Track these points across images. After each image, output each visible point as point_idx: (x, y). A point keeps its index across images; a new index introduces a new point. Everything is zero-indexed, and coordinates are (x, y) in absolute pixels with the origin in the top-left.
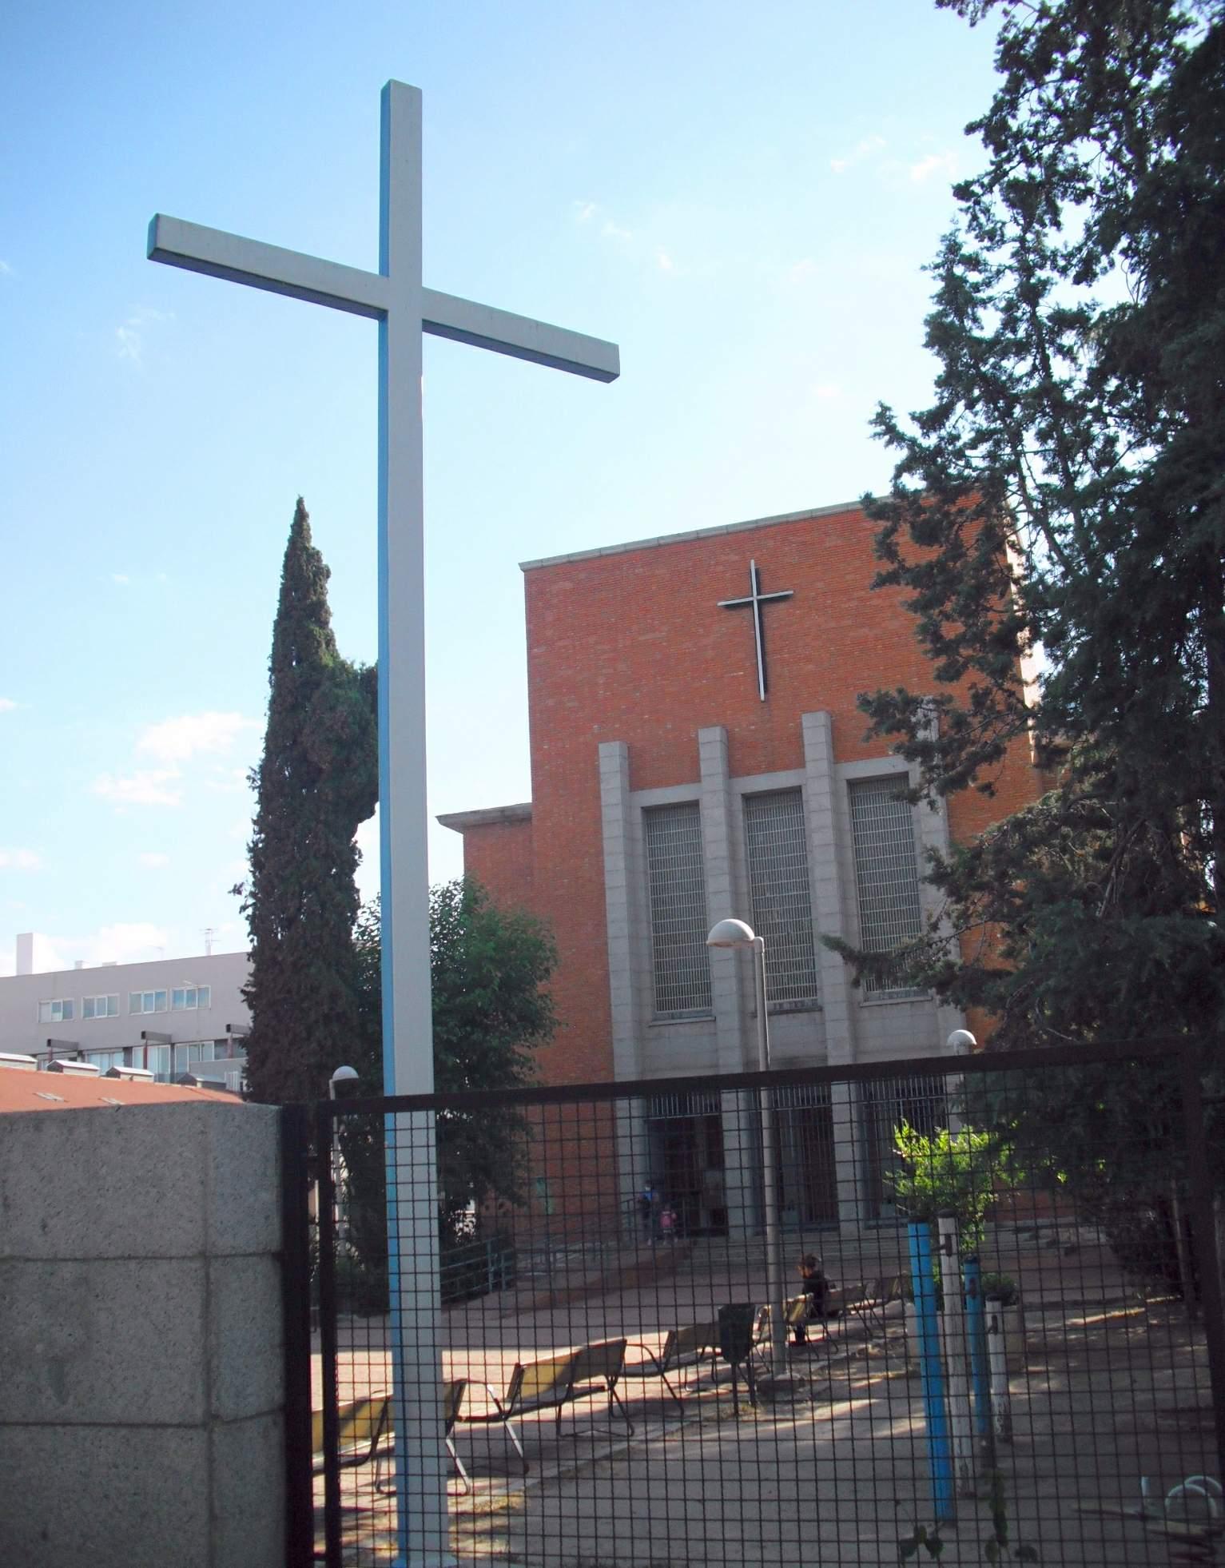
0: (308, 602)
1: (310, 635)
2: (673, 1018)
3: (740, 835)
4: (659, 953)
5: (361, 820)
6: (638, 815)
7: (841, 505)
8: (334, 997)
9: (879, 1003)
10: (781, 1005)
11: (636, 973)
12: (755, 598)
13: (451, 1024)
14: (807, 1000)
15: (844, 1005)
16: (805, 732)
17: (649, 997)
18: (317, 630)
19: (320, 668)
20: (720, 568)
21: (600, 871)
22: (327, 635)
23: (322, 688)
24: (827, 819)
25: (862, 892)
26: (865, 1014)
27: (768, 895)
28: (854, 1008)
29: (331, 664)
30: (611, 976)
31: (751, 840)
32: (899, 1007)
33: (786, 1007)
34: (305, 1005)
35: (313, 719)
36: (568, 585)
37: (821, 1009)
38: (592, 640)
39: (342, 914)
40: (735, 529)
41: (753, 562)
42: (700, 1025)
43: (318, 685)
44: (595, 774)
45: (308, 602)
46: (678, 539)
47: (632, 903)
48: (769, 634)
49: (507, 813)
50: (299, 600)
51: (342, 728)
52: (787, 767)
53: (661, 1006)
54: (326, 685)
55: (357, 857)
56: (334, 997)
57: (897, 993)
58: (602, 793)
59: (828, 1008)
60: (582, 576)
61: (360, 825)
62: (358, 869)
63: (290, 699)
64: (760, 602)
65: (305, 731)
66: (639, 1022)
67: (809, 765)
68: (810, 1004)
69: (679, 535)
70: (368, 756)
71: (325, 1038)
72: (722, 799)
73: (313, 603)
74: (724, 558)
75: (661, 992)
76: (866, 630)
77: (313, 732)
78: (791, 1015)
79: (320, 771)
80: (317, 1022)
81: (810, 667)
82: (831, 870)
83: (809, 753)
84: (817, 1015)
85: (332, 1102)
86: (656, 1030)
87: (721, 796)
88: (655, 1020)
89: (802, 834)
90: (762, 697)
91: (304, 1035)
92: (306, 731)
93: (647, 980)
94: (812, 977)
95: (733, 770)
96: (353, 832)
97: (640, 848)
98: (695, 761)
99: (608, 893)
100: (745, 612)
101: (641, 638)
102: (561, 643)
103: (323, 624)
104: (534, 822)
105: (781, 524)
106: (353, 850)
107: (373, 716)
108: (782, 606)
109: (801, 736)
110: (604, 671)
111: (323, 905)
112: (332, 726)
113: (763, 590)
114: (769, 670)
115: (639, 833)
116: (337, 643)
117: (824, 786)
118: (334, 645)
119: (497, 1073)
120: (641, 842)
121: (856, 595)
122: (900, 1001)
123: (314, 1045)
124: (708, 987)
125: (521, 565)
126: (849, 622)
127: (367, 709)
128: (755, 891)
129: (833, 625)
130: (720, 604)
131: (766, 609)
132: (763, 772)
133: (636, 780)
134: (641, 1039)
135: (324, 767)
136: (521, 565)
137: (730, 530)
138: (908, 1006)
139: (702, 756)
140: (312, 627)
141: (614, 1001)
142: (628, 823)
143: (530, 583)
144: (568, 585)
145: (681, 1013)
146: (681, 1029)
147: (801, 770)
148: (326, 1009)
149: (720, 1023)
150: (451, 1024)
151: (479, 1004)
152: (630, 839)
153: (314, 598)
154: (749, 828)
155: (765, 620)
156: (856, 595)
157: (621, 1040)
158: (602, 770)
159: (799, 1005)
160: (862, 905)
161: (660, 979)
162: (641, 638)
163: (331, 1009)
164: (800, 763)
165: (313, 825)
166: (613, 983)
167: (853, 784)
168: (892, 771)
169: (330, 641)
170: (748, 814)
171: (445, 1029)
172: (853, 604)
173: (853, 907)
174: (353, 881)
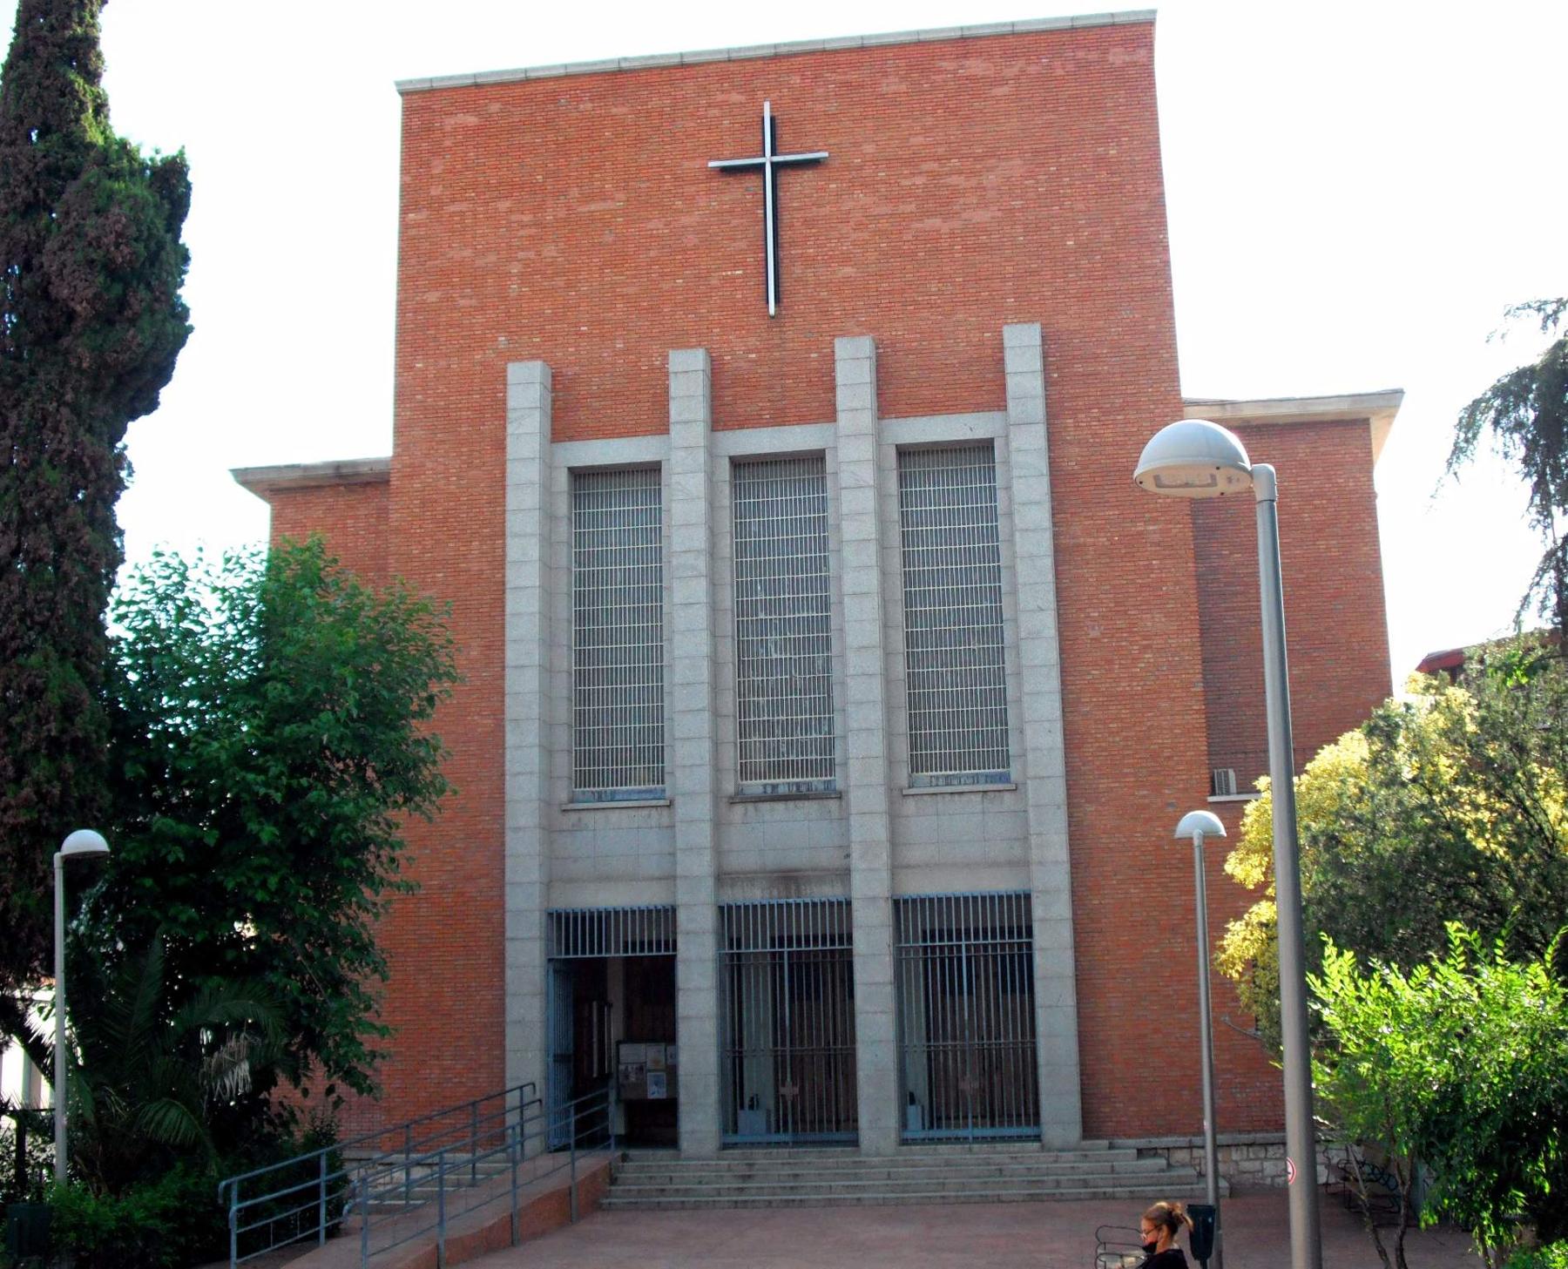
0: (68, 33)
1: (67, 90)
2: (600, 800)
3: (726, 522)
4: (582, 698)
5: (134, 416)
6: (563, 480)
7: (909, 33)
8: (68, 711)
9: (932, 790)
10: (774, 787)
11: (547, 725)
12: (768, 159)
13: (274, 771)
14: (817, 781)
15: (882, 790)
16: (839, 366)
17: (564, 765)
18: (79, 83)
19: (76, 144)
20: (715, 112)
21: (499, 562)
22: (98, 96)
23: (84, 177)
24: (867, 500)
25: (910, 618)
26: (910, 806)
27: (762, 616)
28: (896, 795)
29: (101, 141)
30: (508, 728)
31: (740, 530)
32: (965, 798)
33: (782, 790)
34: (15, 720)
35: (65, 228)
36: (472, 120)
37: (840, 796)
38: (504, 205)
39: (92, 568)
40: (742, 55)
41: (767, 106)
42: (645, 812)
43: (74, 174)
44: (498, 410)
45: (68, 33)
46: (651, 62)
47: (547, 617)
48: (785, 217)
49: (344, 471)
50: (52, 29)
51: (117, 245)
52: (802, 420)
53: (582, 779)
54: (91, 174)
55: (123, 474)
56: (68, 711)
57: (959, 777)
58: (509, 440)
59: (856, 798)
60: (495, 107)
61: (130, 425)
62: (124, 495)
63: (24, 192)
64: (773, 164)
65: (48, 245)
66: (547, 803)
67: (842, 417)
68: (821, 787)
69: (653, 57)
70: (157, 300)
71: (49, 781)
72: (702, 460)
73: (74, 38)
74: (720, 97)
75: (581, 758)
76: (936, 222)
77: (62, 248)
78: (791, 804)
79: (71, 316)
80: (35, 750)
81: (848, 270)
82: (871, 580)
83: (843, 398)
84: (833, 805)
85: (1024, 314)
86: (574, 817)
87: (701, 456)
88: (572, 801)
89: (820, 523)
90: (772, 310)
91: (11, 771)
92: (51, 245)
93: (563, 738)
94: (829, 746)
95: (721, 418)
96: (119, 433)
97: (563, 531)
98: (661, 401)
99: (509, 596)
100: (751, 182)
101: (583, 209)
102: (452, 208)
103: (92, 76)
104: (394, 482)
105: (812, 53)
106: (120, 460)
107: (169, 236)
108: (808, 175)
109: (831, 372)
110: (521, 255)
111: (61, 547)
112: (98, 238)
113: (779, 149)
114: (782, 271)
115: (563, 506)
116: (112, 114)
117: (865, 449)
118: (106, 117)
119: (346, 862)
120: (565, 521)
121: (925, 167)
122: (966, 788)
123: (27, 791)
124: (659, 754)
125: (398, 84)
126: (912, 207)
127: (160, 224)
128: (741, 608)
129: (884, 210)
130: (712, 164)
131: (786, 178)
132: (767, 425)
133: (563, 425)
134: (549, 830)
135: (78, 308)
136: (398, 84)
137: (734, 55)
138: (978, 798)
139: (673, 392)
140: (72, 76)
141: (509, 767)
142: (547, 489)
143: (408, 112)
144: (472, 120)
145: (614, 793)
146: (614, 817)
147: (831, 424)
148: (53, 728)
149: (681, 810)
150: (274, 771)
151: (325, 738)
152: (549, 516)
153: (79, 30)
154: (738, 512)
155: (780, 194)
156: (925, 167)
157: (517, 829)
158: (511, 403)
159: (803, 789)
160: (910, 639)
161: (581, 737)
162: (583, 209)
163: (63, 731)
164: (829, 414)
165: (52, 407)
166: (511, 739)
167: (904, 452)
168: (969, 436)
169: (100, 108)
170: (737, 489)
171: (261, 778)
172: (919, 180)
173: (729, 703)
174: (113, 514)
